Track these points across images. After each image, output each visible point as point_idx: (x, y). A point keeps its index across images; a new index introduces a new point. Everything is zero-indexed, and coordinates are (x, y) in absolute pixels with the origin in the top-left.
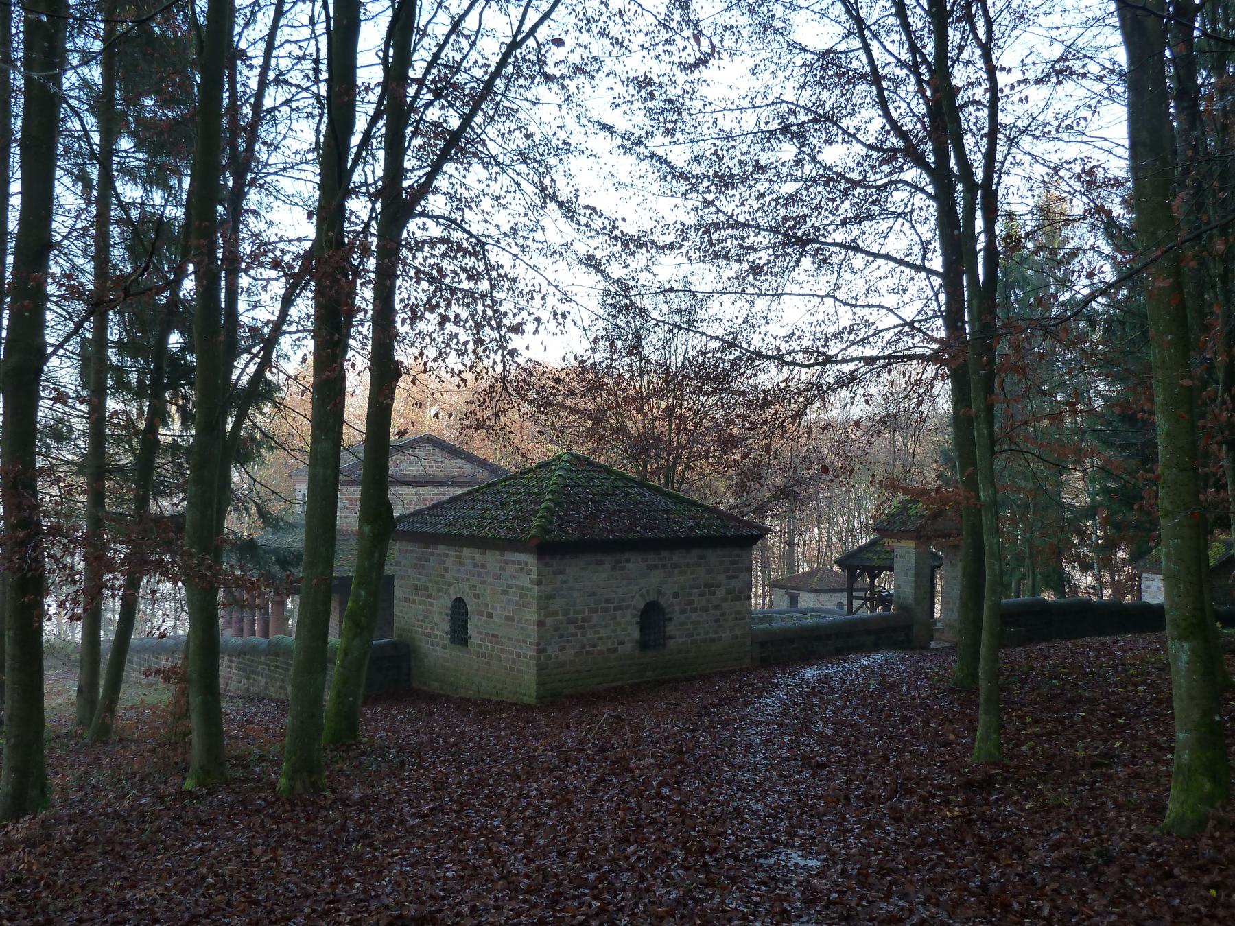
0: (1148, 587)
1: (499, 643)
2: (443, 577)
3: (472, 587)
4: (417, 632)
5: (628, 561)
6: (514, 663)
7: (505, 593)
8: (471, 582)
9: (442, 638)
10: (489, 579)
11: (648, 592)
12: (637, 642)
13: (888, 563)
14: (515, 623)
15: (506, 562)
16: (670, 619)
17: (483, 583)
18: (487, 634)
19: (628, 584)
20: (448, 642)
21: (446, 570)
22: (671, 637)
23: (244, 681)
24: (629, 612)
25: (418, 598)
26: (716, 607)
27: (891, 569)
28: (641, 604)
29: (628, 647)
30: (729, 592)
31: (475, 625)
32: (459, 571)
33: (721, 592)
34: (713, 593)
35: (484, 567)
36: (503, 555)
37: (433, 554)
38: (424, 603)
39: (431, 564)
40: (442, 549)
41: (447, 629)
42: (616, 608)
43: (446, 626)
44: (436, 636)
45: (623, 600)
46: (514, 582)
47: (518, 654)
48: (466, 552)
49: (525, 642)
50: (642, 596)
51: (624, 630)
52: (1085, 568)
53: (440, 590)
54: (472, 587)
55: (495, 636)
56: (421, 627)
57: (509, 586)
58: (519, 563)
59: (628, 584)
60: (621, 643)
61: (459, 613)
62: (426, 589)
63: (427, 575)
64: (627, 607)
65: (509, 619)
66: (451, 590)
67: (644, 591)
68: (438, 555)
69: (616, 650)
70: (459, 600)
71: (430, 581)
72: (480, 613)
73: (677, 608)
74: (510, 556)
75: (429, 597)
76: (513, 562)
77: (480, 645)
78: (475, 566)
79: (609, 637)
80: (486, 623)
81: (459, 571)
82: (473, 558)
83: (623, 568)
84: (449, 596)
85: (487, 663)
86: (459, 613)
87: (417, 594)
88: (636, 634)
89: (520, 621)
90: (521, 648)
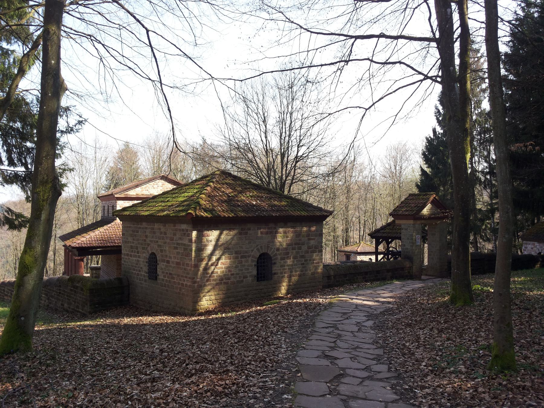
0: (526, 248)
1: (173, 278)
2: (145, 240)
3: (159, 246)
4: (132, 273)
5: (249, 229)
6: (180, 290)
7: (176, 248)
8: (160, 243)
9: (144, 276)
10: (168, 241)
11: (261, 247)
12: (255, 276)
13: (398, 235)
14: (181, 266)
15: (176, 230)
16: (275, 263)
17: (165, 243)
18: (167, 273)
19: (250, 243)
20: (147, 278)
21: (146, 236)
22: (275, 274)
23: (47, 301)
24: (250, 259)
25: (132, 254)
26: (302, 257)
27: (400, 238)
28: (258, 255)
29: (250, 279)
30: (309, 248)
31: (161, 266)
32: (153, 237)
33: (304, 248)
34: (300, 248)
35: (165, 233)
36: (175, 226)
37: (140, 228)
38: (135, 256)
39: (139, 233)
40: (144, 225)
41: (147, 271)
42: (242, 257)
43: (146, 269)
44: (141, 275)
45: (246, 252)
46: (180, 242)
47: (182, 284)
48: (156, 226)
49: (186, 277)
50: (258, 250)
51: (248, 269)
52: (488, 240)
53: (143, 248)
54: (159, 246)
55: (170, 274)
56: (134, 270)
57: (178, 244)
58: (183, 230)
59: (250, 243)
60: (245, 277)
61: (153, 261)
62: (137, 248)
63: (138, 240)
64: (249, 256)
65: (178, 264)
66: (149, 249)
67: (259, 247)
68: (143, 228)
69: (242, 281)
70: (153, 254)
71: (139, 243)
72: (163, 261)
73: (279, 257)
74: (178, 226)
75: (138, 252)
76: (180, 230)
77: (163, 280)
78: (161, 233)
79: (237, 274)
80: (166, 266)
81: (153, 237)
82: (160, 229)
83: (246, 233)
84: (148, 252)
85: (167, 290)
86: (153, 261)
87: (132, 251)
88: (255, 272)
89: (183, 265)
90: (184, 281)
